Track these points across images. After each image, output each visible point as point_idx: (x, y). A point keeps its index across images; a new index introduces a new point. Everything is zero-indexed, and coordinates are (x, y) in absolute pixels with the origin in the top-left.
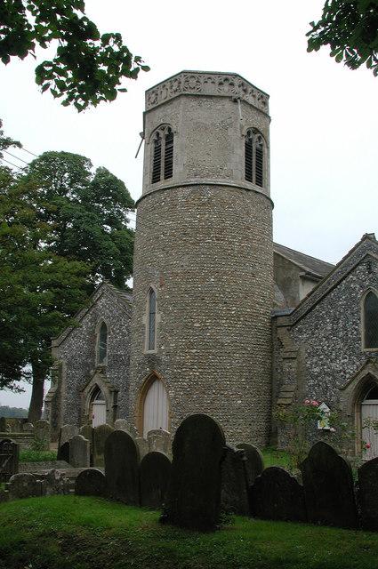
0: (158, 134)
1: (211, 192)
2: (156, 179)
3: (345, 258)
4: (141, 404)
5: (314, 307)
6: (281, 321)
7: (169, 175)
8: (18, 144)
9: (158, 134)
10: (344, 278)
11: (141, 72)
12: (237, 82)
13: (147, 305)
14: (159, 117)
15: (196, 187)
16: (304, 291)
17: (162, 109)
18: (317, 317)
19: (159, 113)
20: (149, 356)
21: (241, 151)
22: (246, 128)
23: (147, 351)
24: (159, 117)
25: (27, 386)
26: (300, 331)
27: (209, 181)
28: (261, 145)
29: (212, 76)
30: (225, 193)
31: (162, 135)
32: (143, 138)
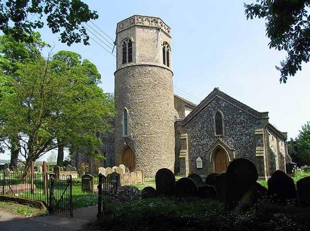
0: (124, 42)
1: (150, 68)
2: (124, 62)
3: (206, 98)
4: (179, 164)
5: (193, 118)
6: (178, 123)
7: (130, 60)
8: (49, 46)
9: (124, 42)
10: (206, 106)
11: (97, 13)
12: (159, 21)
13: (123, 116)
14: (124, 35)
15: (160, 69)
16: (187, 112)
17: (126, 31)
18: (195, 122)
19: (125, 33)
20: (125, 138)
21: (162, 52)
22: (163, 42)
23: (124, 136)
24: (124, 35)
25: (56, 151)
26: (187, 127)
27: (147, 63)
28: (168, 50)
29: (149, 18)
30: (155, 69)
31: (126, 42)
32: (115, 45)
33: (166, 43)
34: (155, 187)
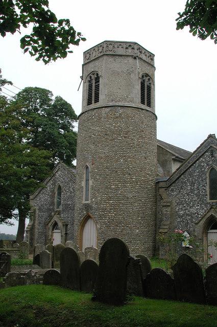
0: (91, 77)
1: (121, 111)
2: (89, 103)
3: (198, 148)
4: (81, 232)
5: (180, 176)
6: (161, 184)
7: (97, 100)
8: (11, 83)
9: (91, 77)
10: (197, 160)
12: (136, 47)
13: (85, 175)
14: (91, 68)
16: (175, 167)
17: (93, 63)
19: (91, 65)
20: (85, 205)
21: (139, 87)
22: (141, 73)
23: (84, 202)
24: (91, 68)
25: (15, 222)
26: (172, 190)
27: (120, 104)
28: (150, 84)
29: (122, 44)
30: (129, 111)
31: (93, 78)
32: (82, 79)
33: (147, 75)
34: (98, 263)
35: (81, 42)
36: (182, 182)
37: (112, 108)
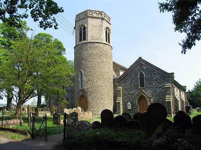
0: (81, 28)
2: (81, 40)
3: (134, 64)
4: (116, 106)
5: (125, 76)
6: (116, 80)
7: (85, 39)
8: (32, 30)
9: (81, 28)
10: (134, 69)
12: (103, 14)
13: (80, 76)
14: (81, 23)
17: (82, 20)
19: (81, 21)
20: (81, 89)
21: (105, 33)
23: (80, 88)
24: (81, 23)
25: (36, 98)
26: (122, 83)
27: (95, 41)
28: (109, 32)
29: (96, 12)
30: (101, 45)
31: (82, 28)
32: (75, 29)
33: (108, 28)
35: (63, 9)
36: (127, 79)
37: (104, 45)
